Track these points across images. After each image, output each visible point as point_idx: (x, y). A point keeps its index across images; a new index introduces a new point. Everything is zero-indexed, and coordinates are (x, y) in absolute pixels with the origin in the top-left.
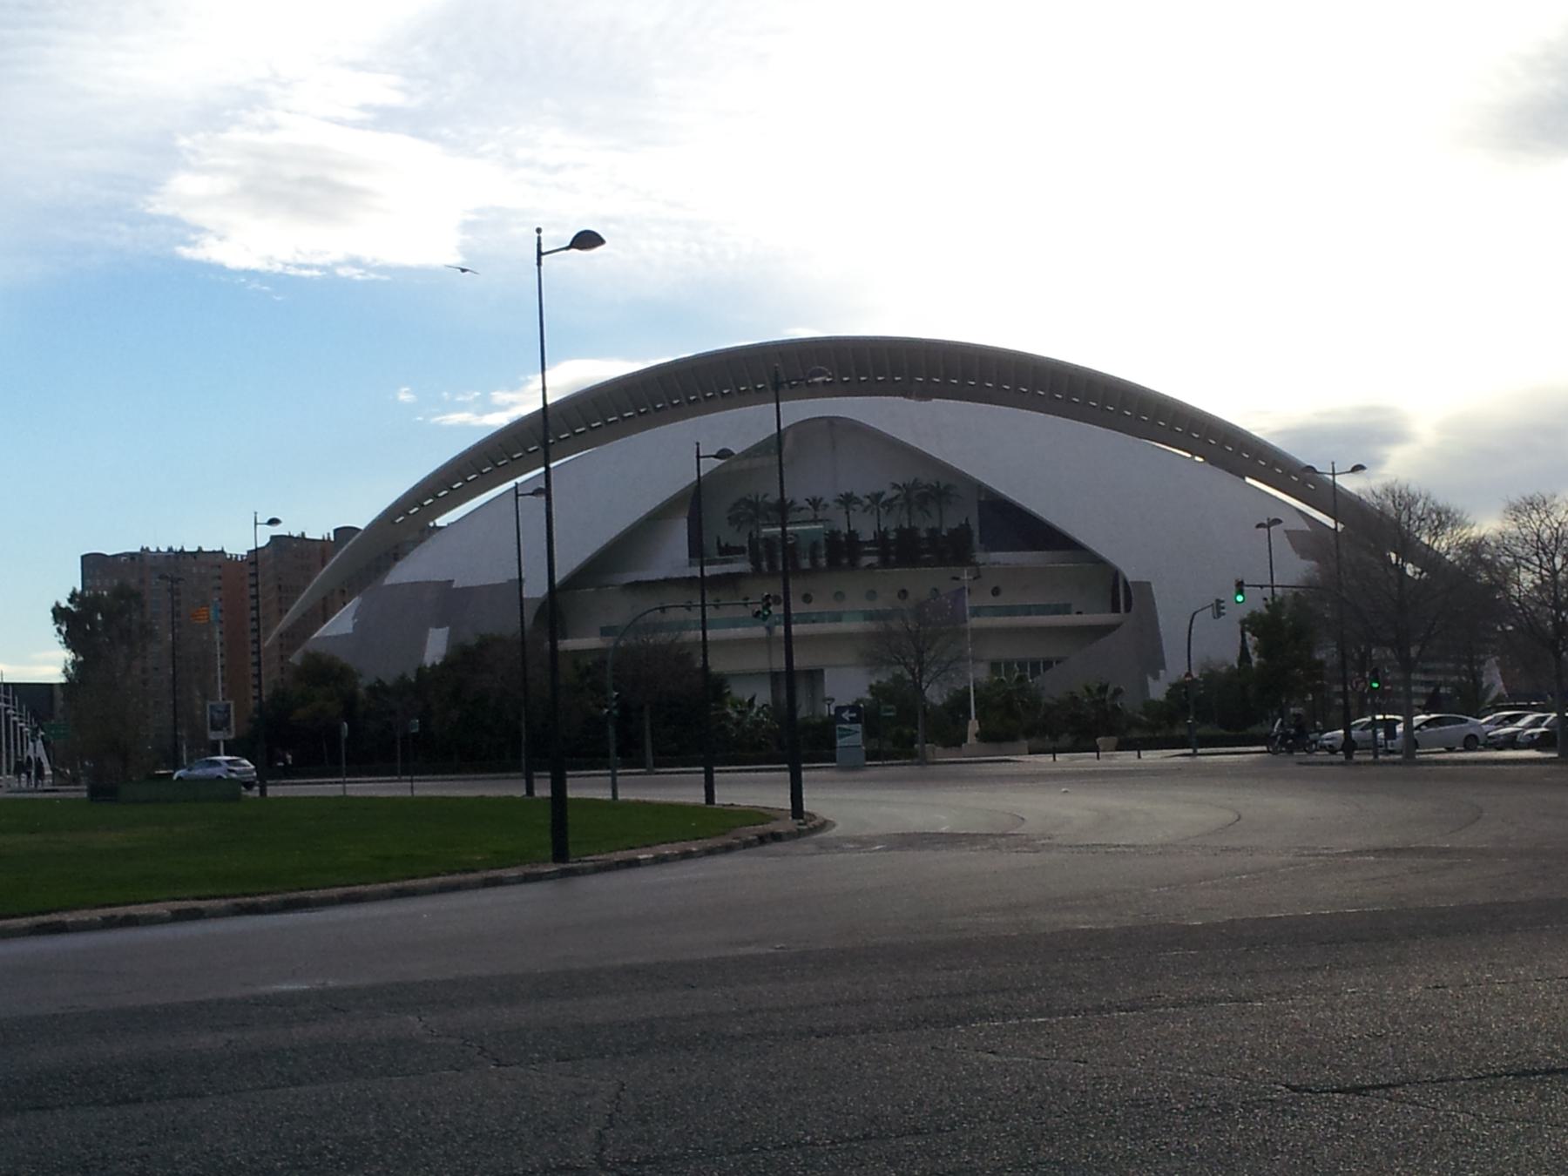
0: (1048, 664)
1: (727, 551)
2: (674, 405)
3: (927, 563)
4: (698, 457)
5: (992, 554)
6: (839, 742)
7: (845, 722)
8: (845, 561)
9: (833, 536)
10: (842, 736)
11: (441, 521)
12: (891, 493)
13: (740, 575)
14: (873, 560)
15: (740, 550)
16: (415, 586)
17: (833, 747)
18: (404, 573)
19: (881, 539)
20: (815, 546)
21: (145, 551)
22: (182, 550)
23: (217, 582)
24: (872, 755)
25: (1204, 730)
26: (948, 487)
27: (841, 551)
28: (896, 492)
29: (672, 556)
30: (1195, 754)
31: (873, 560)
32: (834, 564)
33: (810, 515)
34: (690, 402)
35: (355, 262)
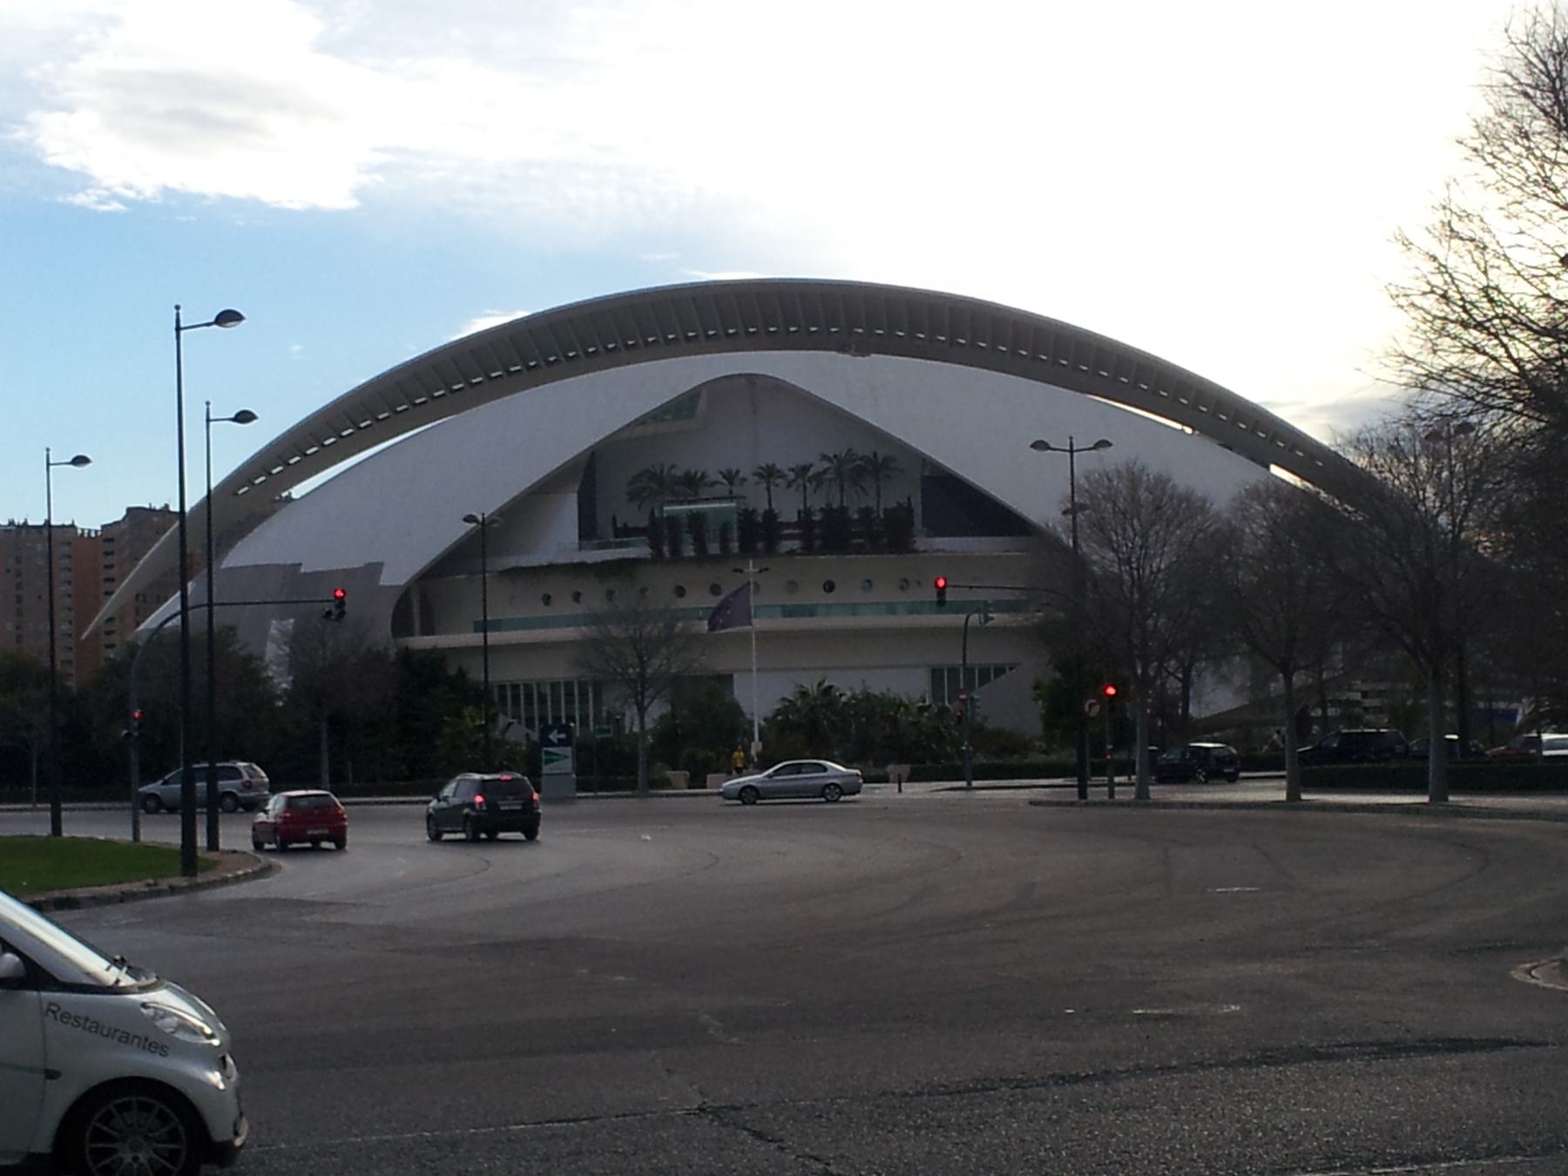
0: (1000, 671)
1: (625, 533)
2: (728, 335)
3: (859, 550)
4: (48, 464)
5: (938, 540)
6: (546, 769)
7: (552, 744)
8: (760, 545)
9: (747, 516)
10: (548, 762)
11: (297, 491)
13: (636, 561)
14: (795, 544)
15: (637, 531)
16: (260, 571)
18: (244, 555)
19: (805, 516)
20: (725, 528)
24: (582, 786)
25: (981, 759)
26: (886, 459)
27: (758, 534)
28: (826, 465)
29: (559, 537)
30: (969, 788)
31: (795, 544)
33: (723, 489)
34: (627, 347)
35: (129, 187)
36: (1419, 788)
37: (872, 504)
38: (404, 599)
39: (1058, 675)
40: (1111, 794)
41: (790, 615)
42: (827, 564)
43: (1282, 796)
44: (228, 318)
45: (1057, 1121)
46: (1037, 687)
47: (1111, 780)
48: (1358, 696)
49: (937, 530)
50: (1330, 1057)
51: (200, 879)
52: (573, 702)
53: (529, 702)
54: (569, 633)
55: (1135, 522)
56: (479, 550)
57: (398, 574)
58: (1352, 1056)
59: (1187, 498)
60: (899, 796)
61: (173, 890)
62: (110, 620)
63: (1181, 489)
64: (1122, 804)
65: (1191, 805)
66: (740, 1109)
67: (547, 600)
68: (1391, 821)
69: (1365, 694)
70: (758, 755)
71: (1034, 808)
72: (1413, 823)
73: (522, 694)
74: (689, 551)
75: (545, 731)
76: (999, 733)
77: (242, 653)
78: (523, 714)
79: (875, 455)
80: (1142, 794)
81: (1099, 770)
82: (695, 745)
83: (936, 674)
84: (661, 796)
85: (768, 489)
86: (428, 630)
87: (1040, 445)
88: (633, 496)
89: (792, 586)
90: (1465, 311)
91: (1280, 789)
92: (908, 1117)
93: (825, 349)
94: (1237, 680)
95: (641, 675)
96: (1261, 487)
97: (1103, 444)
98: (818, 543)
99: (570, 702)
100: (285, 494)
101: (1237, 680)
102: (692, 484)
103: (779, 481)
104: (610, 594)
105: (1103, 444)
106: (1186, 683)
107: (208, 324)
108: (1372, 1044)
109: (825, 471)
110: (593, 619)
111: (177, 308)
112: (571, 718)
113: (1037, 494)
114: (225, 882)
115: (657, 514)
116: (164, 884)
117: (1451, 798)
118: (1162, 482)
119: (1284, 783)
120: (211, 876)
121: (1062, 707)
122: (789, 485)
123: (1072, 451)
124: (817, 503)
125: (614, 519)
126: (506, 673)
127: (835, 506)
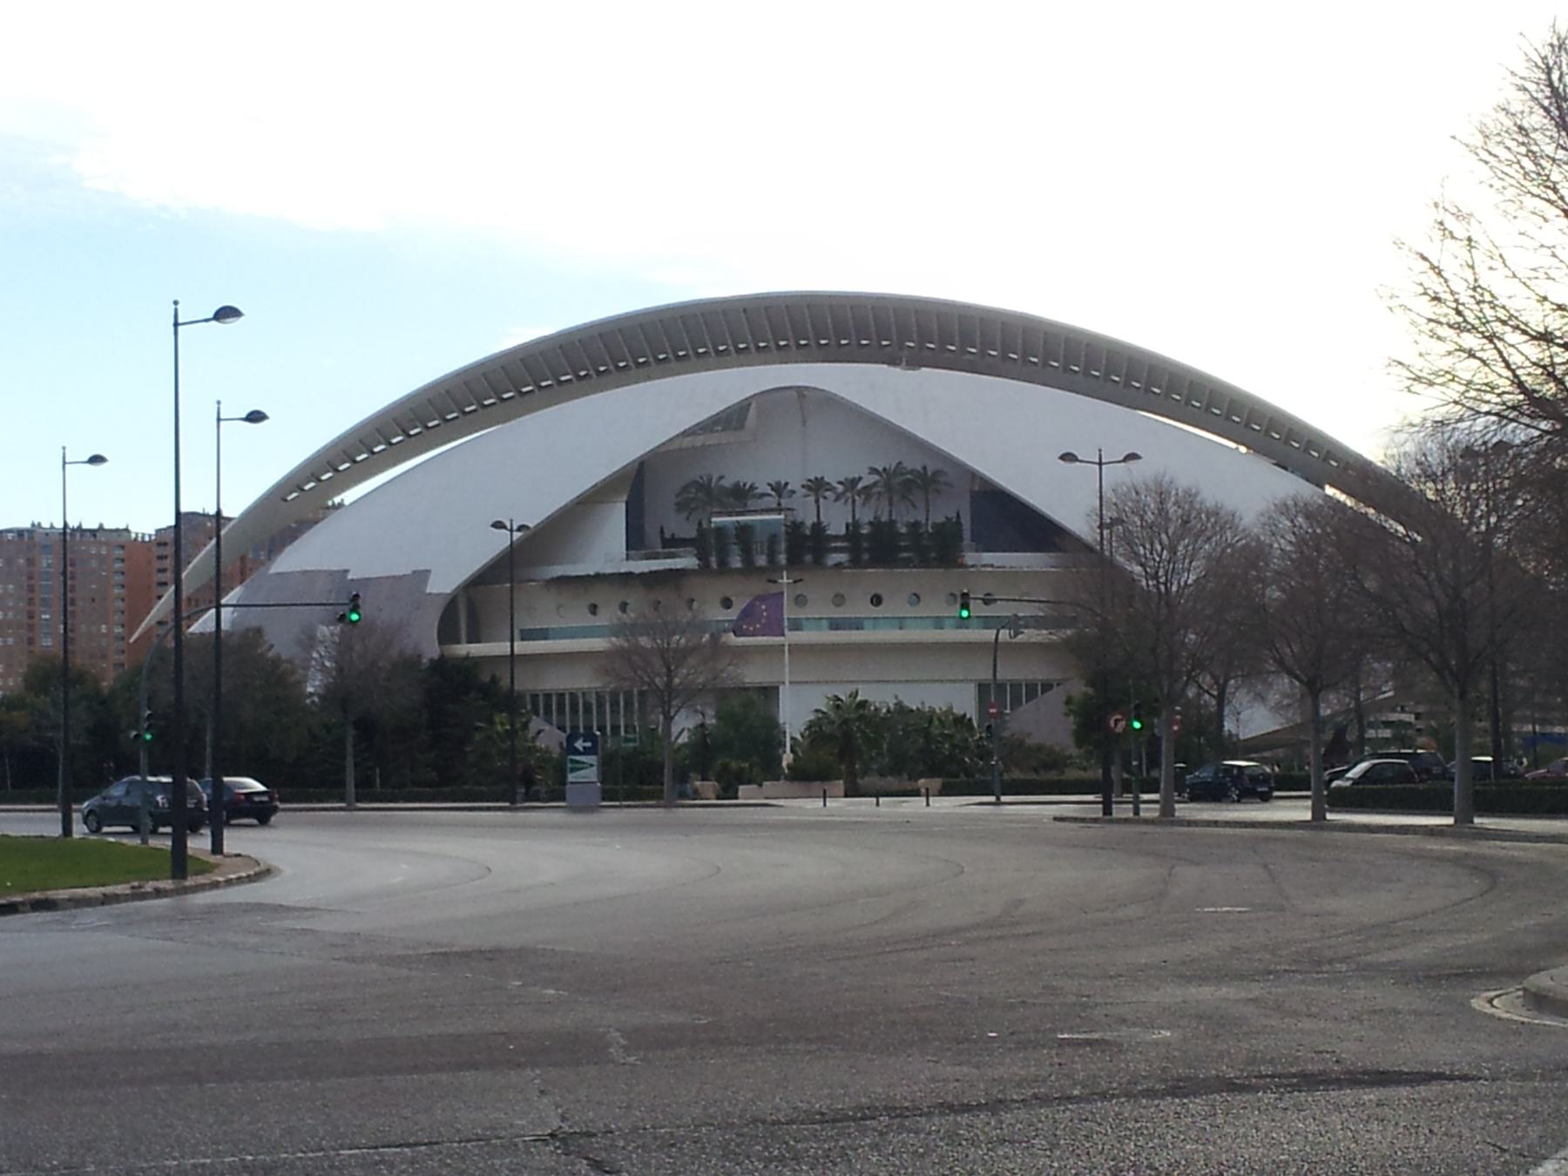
1: (672, 544)
3: (907, 563)
5: (985, 555)
6: (571, 777)
8: (808, 558)
9: (795, 528)
10: (572, 770)
11: (349, 496)
12: (869, 480)
14: (842, 557)
15: (684, 542)
17: (563, 782)
18: (291, 560)
19: (853, 530)
20: (773, 540)
21: (36, 527)
22: (101, 528)
23: (118, 565)
24: (606, 796)
25: (1017, 774)
26: (937, 473)
27: (805, 546)
28: (877, 477)
29: (606, 547)
30: (998, 803)
31: (842, 557)
32: (794, 561)
33: (772, 502)
36: (1445, 810)
37: (921, 517)
38: (450, 607)
39: (1090, 691)
40: (1137, 812)
41: (837, 629)
42: (876, 578)
43: (1308, 816)
44: (226, 313)
45: (922, 1155)
46: (1068, 701)
47: (1137, 797)
48: (1410, 718)
49: (987, 544)
50: (1243, 1089)
51: (189, 882)
52: (632, 713)
53: (561, 711)
54: (597, 644)
55: (1164, 536)
56: (524, 561)
57: (446, 581)
58: (1265, 1089)
59: (1215, 513)
60: (927, 810)
61: (159, 893)
62: (160, 623)
63: (1210, 503)
64: (1147, 822)
65: (1216, 823)
66: (594, 1135)
67: (594, 609)
68: (1411, 842)
69: (1418, 716)
70: (789, 766)
71: (1058, 824)
72: (1434, 845)
73: (556, 705)
74: (736, 562)
75: (572, 738)
76: (1040, 748)
77: (270, 654)
78: (568, 724)
79: (925, 468)
80: (1167, 811)
81: (1127, 788)
82: (737, 756)
83: (983, 688)
84: (683, 806)
85: (817, 501)
86: (474, 638)
87: (1068, 457)
88: (680, 507)
89: (839, 600)
90: (1459, 313)
91: (1306, 808)
92: (766, 1148)
93: (876, 362)
94: (1273, 698)
95: (669, 684)
96: (1290, 503)
97: (1132, 457)
98: (866, 556)
99: (615, 711)
100: (337, 500)
101: (1273, 698)
102: (741, 495)
103: (828, 494)
104: (623, 607)
105: (1132, 457)
106: (1221, 700)
107: (207, 320)
108: (1294, 1076)
109: (875, 484)
110: (616, 630)
111: (176, 303)
112: (602, 728)
113: (1070, 503)
114: (215, 885)
115: (705, 525)
116: (149, 887)
117: (1477, 820)
118: (1191, 496)
119: (1309, 803)
120: (201, 880)
121: (1090, 721)
122: (837, 499)
123: (1100, 464)
124: (865, 516)
125: (662, 532)
126: (527, 683)
127: (884, 518)
